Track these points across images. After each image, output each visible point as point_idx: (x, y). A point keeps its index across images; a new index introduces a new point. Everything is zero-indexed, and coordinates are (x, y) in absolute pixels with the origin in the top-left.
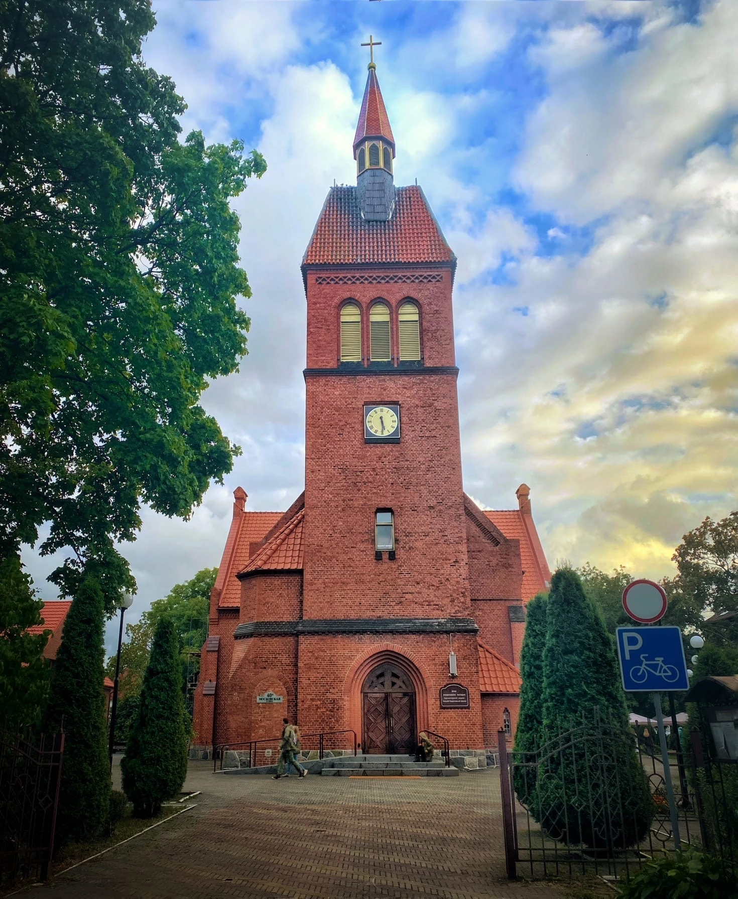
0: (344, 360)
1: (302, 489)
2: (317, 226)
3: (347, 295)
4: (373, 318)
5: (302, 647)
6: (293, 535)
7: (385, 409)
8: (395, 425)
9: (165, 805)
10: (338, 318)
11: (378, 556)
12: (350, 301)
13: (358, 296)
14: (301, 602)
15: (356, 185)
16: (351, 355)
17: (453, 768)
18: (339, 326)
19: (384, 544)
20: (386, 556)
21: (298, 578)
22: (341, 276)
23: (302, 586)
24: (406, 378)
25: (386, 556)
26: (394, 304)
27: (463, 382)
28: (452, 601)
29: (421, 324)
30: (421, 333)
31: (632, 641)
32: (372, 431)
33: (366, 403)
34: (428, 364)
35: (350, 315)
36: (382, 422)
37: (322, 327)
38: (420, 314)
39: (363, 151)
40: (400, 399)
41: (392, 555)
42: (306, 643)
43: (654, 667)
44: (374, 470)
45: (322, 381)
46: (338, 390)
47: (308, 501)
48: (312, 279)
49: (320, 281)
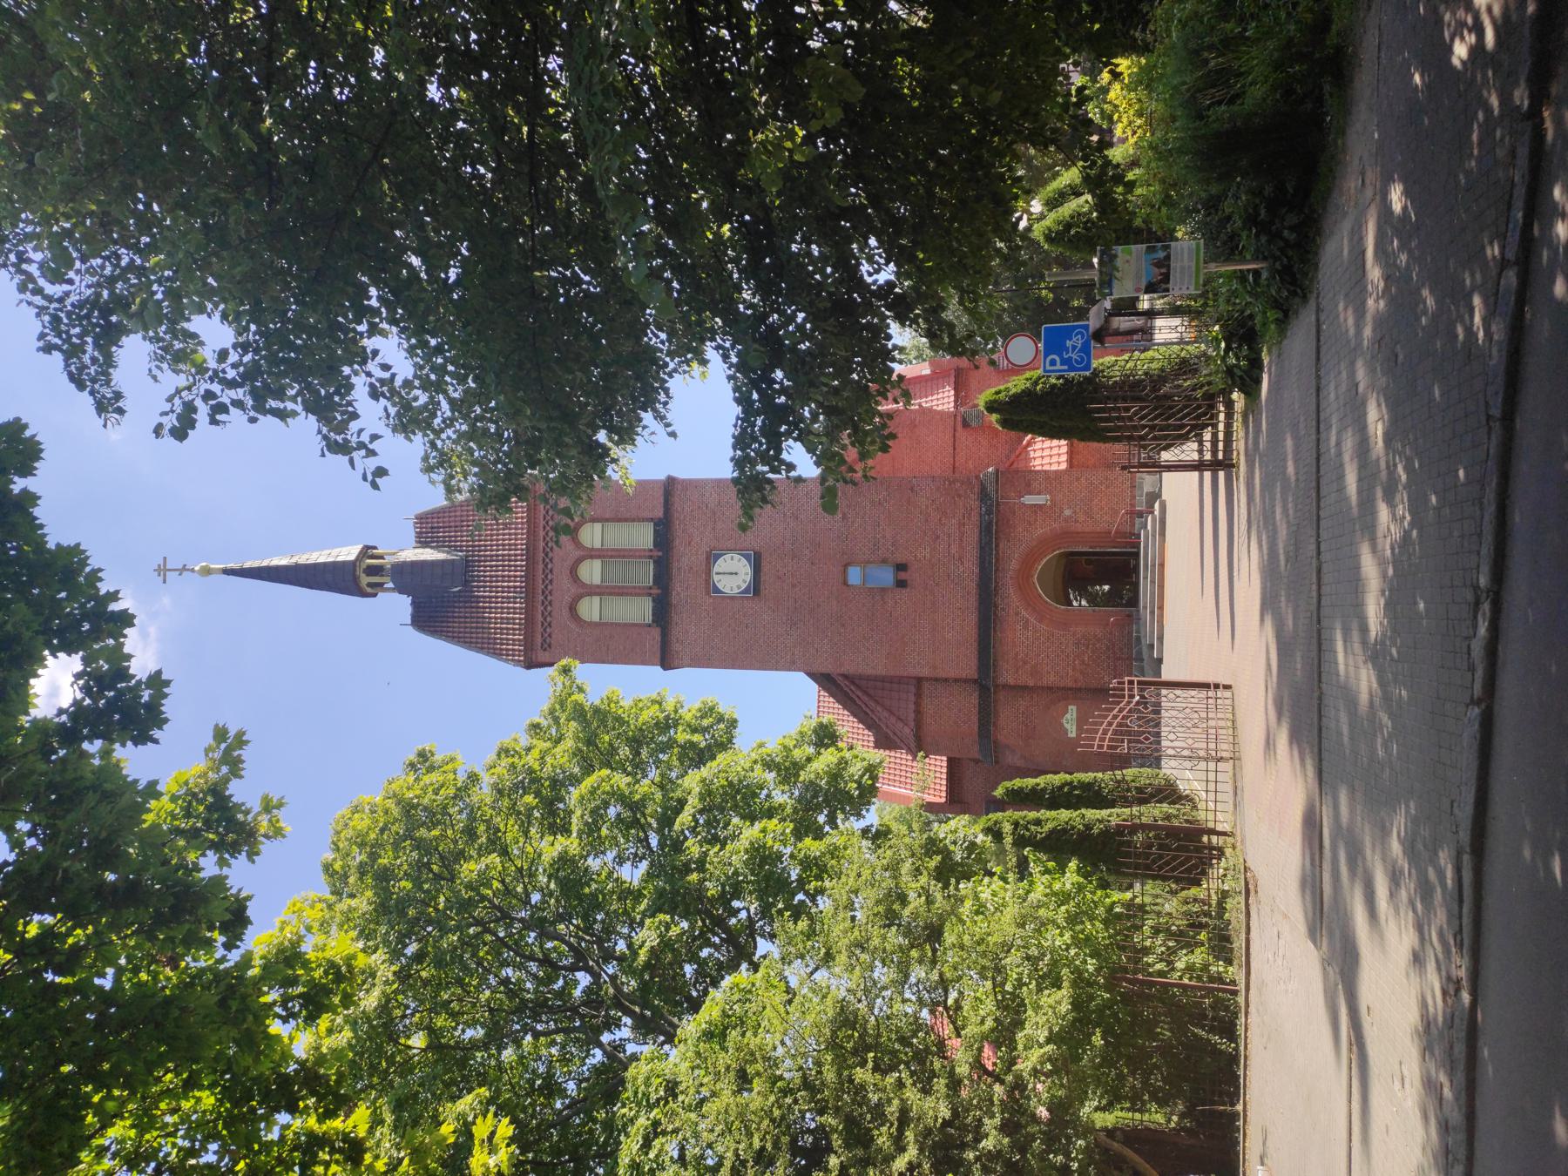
0: (649, 619)
1: (801, 675)
2: (469, 648)
3: (565, 613)
4: (597, 580)
5: (1011, 682)
6: (871, 692)
7: (749, 578)
8: (737, 557)
9: (1342, 678)
10: (596, 624)
11: (901, 584)
12: (572, 609)
13: (568, 599)
14: (956, 680)
15: (51, 545)
16: (640, 610)
17: (1157, 505)
18: (606, 624)
19: (886, 576)
20: (902, 575)
21: (926, 685)
22: (541, 619)
23: (936, 680)
24: (677, 542)
25: (902, 575)
26: (578, 553)
27: (681, 474)
28: (959, 496)
29: (607, 520)
30: (619, 520)
31: (1053, 363)
32: (744, 586)
33: (708, 593)
34: (659, 513)
35: (590, 609)
36: (733, 574)
37: (610, 645)
38: (594, 520)
39: (369, 585)
40: (705, 548)
41: (901, 567)
42: (1008, 676)
43: (1074, 348)
44: (794, 586)
45: (676, 647)
46: (685, 626)
47: (828, 668)
48: (543, 656)
49: (547, 646)
